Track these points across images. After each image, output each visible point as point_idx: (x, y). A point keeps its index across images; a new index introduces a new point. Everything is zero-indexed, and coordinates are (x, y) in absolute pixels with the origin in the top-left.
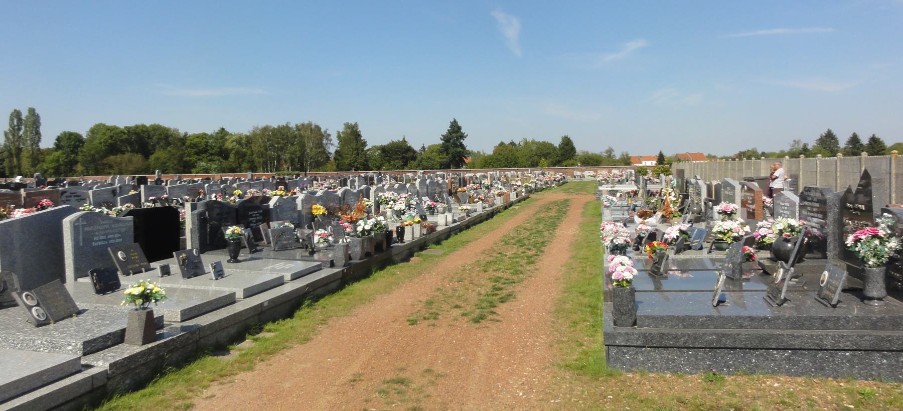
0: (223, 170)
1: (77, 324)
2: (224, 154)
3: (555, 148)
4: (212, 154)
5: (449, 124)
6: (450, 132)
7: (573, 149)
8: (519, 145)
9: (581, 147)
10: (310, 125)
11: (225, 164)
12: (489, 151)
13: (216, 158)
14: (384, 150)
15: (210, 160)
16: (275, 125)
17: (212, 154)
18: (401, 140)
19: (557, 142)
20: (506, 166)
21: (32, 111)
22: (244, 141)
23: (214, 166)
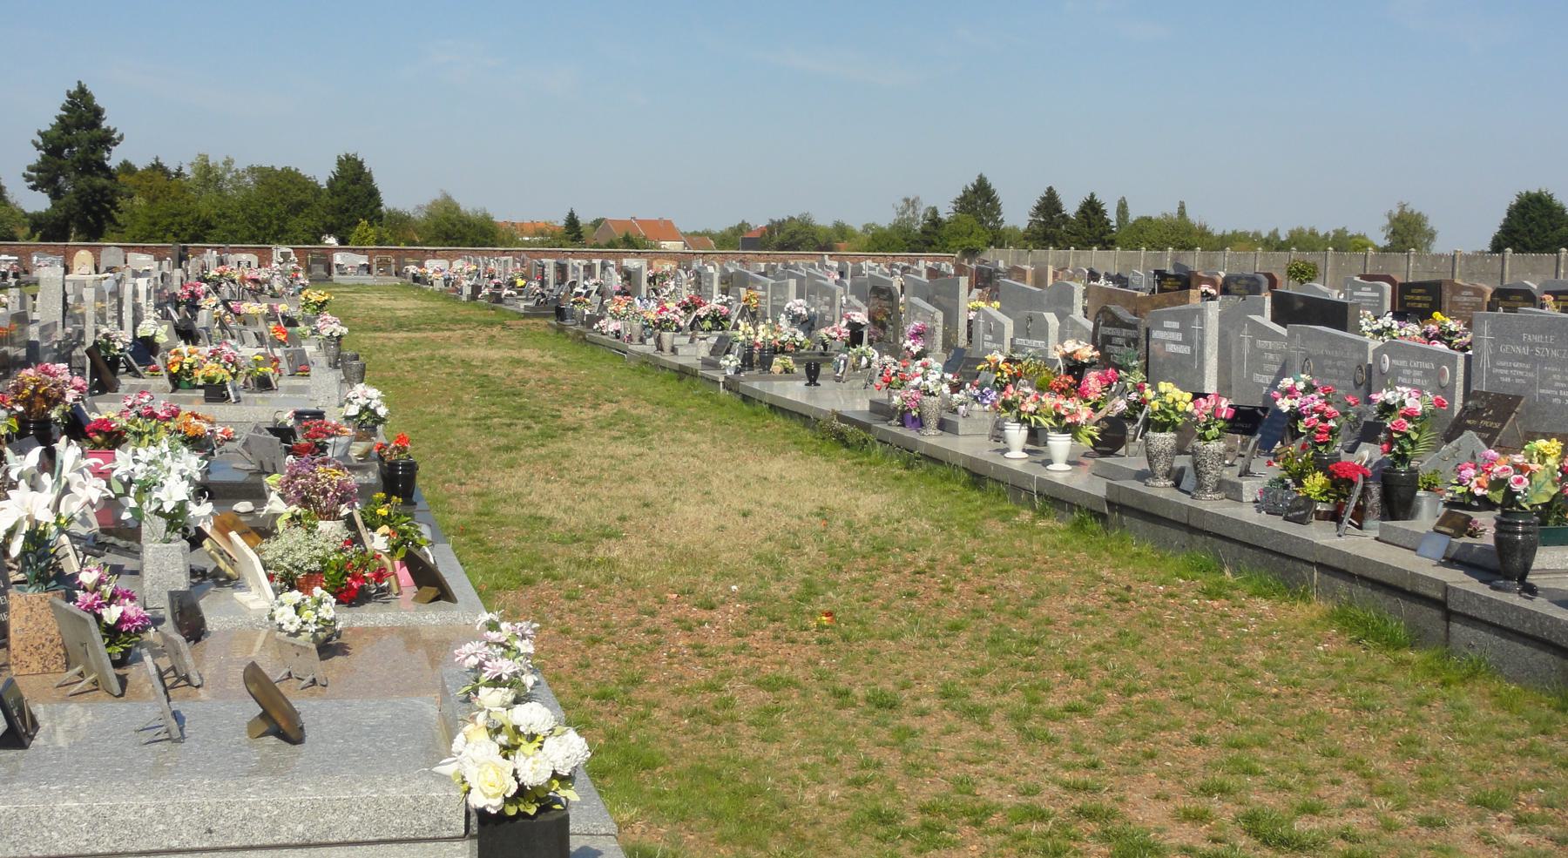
3: (317, 191)
5: (64, 99)
7: (373, 194)
8: (179, 174)
9: (400, 194)
19: (321, 171)
21: (121, 138)
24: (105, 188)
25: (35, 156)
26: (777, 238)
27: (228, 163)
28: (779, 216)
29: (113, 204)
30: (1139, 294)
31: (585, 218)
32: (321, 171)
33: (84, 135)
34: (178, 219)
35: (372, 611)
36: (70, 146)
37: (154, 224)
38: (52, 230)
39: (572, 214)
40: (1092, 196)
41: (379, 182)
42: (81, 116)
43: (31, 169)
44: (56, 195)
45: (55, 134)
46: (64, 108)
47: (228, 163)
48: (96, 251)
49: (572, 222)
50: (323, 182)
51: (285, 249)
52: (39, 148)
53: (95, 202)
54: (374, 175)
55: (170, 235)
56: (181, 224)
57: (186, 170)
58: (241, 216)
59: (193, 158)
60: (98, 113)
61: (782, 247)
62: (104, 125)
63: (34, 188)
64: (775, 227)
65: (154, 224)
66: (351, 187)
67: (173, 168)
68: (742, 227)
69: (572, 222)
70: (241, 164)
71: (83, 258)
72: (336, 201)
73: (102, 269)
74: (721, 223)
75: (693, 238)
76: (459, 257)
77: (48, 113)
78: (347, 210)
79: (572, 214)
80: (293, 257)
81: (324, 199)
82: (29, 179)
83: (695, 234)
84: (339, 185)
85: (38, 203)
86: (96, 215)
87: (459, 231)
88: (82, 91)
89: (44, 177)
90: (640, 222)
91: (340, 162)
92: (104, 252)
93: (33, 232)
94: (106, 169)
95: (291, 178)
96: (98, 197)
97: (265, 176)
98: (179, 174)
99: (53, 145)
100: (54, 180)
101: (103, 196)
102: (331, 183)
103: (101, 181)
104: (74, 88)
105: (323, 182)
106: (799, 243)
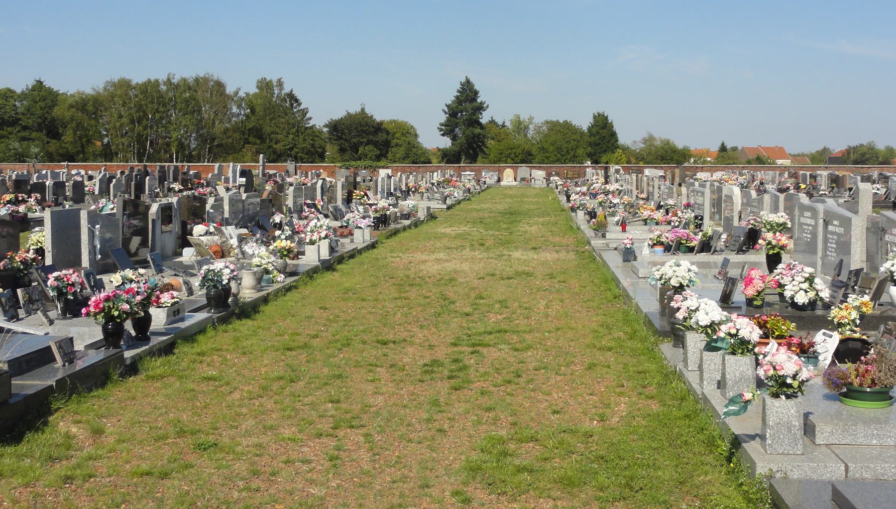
0: (51, 158)
1: (276, 306)
2: (52, 129)
3: (582, 134)
4: (25, 128)
5: (459, 86)
6: (459, 101)
7: (613, 135)
8: (503, 126)
9: (629, 135)
10: (206, 80)
11: (53, 145)
12: (639, 146)
13: (34, 135)
14: (335, 127)
15: (24, 139)
16: (138, 78)
17: (25, 128)
18: (359, 110)
19: (584, 122)
20: (558, 161)
21: (488, 106)
22: (90, 108)
23: (35, 150)
24: (480, 134)
25: (443, 118)
26: (852, 157)
27: (531, 119)
28: (854, 144)
29: (483, 142)
30: (468, 173)
31: (729, 146)
32: (584, 122)
33: (468, 106)
34: (514, 151)
35: (60, 334)
36: (461, 112)
37: (502, 154)
38: (450, 157)
39: (723, 144)
40: (363, 110)
41: (617, 128)
42: (468, 95)
43: (442, 125)
44: (454, 139)
45: (454, 106)
46: (458, 91)
47: (531, 119)
48: (515, 169)
49: (723, 149)
50: (585, 128)
51: (617, 167)
52: (446, 113)
53: (475, 142)
54: (614, 124)
55: (509, 160)
56: (515, 153)
57: (508, 124)
58: (551, 148)
59: (512, 117)
60: (476, 93)
61: (856, 162)
62: (479, 100)
63: (443, 135)
64: (848, 151)
65: (502, 154)
66: (601, 131)
67: (500, 123)
68: (825, 150)
69: (723, 149)
70: (539, 119)
71: (508, 173)
72: (592, 139)
73: (518, 179)
74: (814, 148)
75: (795, 157)
76: (717, 171)
77: (450, 95)
78: (599, 144)
79: (723, 144)
80: (621, 171)
81: (586, 138)
82: (441, 130)
83: (799, 155)
84: (594, 130)
85: (446, 143)
86: (474, 150)
87: (669, 157)
88: (468, 81)
89: (448, 129)
90: (764, 148)
91: (595, 117)
92: (519, 170)
93: (443, 158)
94: (480, 124)
95: (567, 126)
96: (476, 139)
97: (554, 126)
98: (503, 126)
99: (453, 112)
100: (453, 131)
101: (479, 138)
102: (589, 129)
103: (477, 131)
104: (464, 80)
105: (585, 128)
106: (868, 159)
